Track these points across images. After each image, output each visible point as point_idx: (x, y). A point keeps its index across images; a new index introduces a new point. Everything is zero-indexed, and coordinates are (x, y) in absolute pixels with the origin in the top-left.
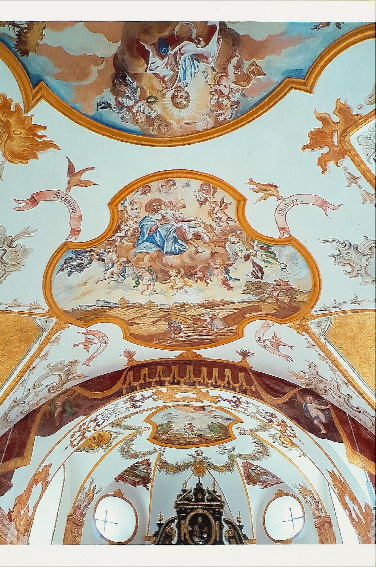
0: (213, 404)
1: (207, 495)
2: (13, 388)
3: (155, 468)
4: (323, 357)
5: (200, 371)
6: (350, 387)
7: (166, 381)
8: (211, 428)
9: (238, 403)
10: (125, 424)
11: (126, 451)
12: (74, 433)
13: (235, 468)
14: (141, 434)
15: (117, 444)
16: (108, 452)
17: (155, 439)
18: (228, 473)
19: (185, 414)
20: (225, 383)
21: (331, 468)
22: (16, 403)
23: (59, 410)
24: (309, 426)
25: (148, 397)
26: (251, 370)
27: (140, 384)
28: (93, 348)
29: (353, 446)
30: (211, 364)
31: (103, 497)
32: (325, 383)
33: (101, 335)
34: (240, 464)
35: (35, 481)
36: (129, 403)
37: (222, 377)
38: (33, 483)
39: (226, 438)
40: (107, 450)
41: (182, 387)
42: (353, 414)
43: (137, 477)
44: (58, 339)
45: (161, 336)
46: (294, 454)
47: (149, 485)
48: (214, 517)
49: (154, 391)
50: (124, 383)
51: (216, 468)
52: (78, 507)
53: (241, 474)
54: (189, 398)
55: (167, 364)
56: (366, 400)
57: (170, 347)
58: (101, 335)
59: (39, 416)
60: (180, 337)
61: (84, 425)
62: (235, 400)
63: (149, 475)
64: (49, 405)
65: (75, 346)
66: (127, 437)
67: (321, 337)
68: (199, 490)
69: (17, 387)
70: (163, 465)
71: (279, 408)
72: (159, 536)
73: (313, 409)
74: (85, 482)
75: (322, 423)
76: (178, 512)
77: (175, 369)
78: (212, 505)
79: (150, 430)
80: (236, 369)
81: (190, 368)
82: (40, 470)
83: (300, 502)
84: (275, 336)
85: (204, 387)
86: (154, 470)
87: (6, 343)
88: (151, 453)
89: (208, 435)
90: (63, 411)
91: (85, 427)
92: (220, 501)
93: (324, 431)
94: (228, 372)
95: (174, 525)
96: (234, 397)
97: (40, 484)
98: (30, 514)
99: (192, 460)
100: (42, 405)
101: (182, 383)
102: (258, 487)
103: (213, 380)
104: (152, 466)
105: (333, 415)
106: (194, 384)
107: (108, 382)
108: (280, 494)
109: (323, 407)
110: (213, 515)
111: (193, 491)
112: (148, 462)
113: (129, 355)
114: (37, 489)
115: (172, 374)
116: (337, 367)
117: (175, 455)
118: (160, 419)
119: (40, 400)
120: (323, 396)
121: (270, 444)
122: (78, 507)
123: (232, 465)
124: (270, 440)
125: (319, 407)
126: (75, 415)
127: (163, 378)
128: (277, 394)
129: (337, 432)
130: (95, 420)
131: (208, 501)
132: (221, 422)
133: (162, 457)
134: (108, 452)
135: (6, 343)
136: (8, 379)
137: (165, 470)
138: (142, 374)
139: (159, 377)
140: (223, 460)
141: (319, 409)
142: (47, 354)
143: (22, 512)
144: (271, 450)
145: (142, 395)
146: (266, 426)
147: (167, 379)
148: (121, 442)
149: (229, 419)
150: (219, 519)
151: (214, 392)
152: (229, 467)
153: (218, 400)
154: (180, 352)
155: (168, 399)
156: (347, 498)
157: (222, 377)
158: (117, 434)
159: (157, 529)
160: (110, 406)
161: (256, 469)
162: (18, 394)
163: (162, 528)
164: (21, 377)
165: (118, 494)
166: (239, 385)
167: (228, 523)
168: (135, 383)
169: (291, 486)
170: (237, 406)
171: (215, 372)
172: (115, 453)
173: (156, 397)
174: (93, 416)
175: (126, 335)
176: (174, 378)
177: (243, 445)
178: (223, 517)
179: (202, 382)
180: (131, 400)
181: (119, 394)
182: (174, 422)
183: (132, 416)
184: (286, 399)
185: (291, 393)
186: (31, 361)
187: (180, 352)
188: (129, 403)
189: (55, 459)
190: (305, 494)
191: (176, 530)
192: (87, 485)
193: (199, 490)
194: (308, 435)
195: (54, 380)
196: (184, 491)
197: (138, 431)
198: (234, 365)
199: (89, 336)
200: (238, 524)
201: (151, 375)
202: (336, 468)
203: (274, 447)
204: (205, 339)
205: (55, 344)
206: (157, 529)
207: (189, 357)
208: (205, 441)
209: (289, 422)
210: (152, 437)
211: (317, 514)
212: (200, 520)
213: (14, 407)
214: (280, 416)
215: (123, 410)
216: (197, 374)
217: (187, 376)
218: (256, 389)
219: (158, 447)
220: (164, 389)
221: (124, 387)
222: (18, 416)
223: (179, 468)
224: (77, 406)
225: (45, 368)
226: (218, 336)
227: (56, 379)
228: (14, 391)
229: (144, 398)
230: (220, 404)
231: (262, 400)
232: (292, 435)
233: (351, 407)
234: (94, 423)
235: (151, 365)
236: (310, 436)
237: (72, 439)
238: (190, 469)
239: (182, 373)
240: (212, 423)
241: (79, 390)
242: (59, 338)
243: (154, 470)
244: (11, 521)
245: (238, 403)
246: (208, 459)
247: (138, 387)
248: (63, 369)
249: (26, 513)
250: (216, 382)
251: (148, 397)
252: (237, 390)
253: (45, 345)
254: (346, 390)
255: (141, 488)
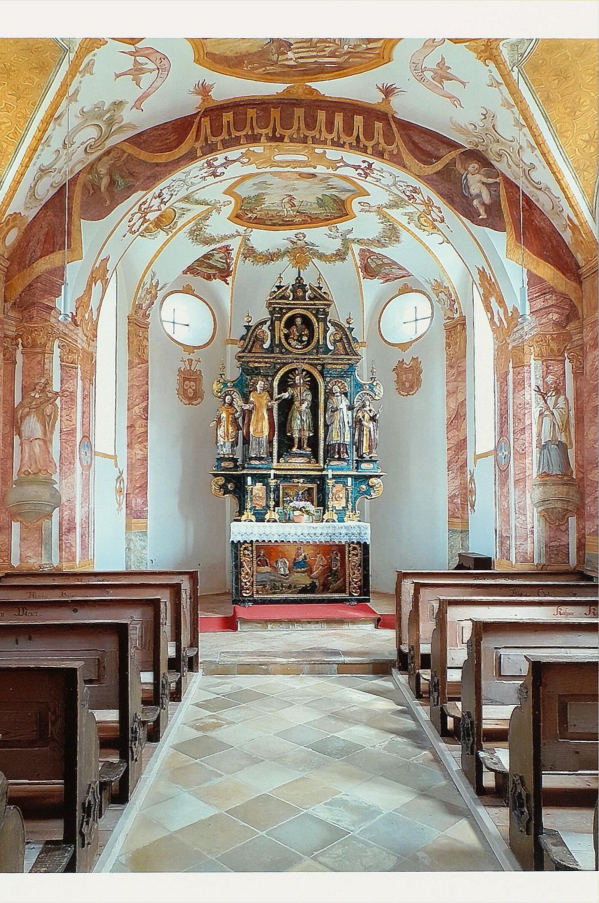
0: (331, 171)
1: (309, 292)
2: (35, 150)
3: (238, 258)
4: (508, 103)
5: (314, 119)
6: (538, 152)
7: (261, 135)
8: (321, 203)
9: (368, 171)
10: (196, 197)
11: (197, 235)
12: (133, 215)
13: (349, 257)
14: (219, 211)
15: (184, 226)
16: (172, 237)
17: (237, 217)
18: (338, 263)
19: (284, 183)
20: (352, 140)
21: (482, 263)
22: (44, 171)
23: (105, 182)
24: (464, 205)
25: (235, 161)
26: (393, 117)
27: (221, 141)
28: (147, 79)
29: (518, 239)
30: (334, 106)
31: (172, 293)
32: (503, 143)
33: (159, 56)
34: (357, 252)
35: (93, 280)
36: (206, 170)
37: (349, 128)
38: (91, 281)
39: (341, 217)
40: (171, 234)
41: (286, 145)
42: (530, 192)
43: (212, 267)
44: (91, 64)
45: (256, 58)
46: (433, 240)
47: (229, 279)
48: (316, 317)
49: (244, 151)
50: (197, 138)
51: (322, 257)
52: (140, 307)
53: (356, 264)
54: (295, 161)
55: (263, 105)
56: (554, 173)
57: (269, 77)
58: (159, 56)
59: (78, 189)
60: (287, 59)
61: (144, 203)
62: (363, 165)
63: (229, 267)
64: (88, 173)
65: (118, 76)
66: (199, 215)
67: (515, 69)
68: (299, 285)
69: (40, 147)
70: (249, 253)
71: (428, 180)
72: (247, 340)
73: (475, 182)
74: (143, 276)
75: (484, 204)
76: (271, 313)
77: (275, 113)
78: (315, 304)
79: (232, 206)
80: (374, 115)
81: (299, 112)
82: (97, 265)
83: (430, 300)
84: (442, 64)
85: (321, 146)
86: (237, 260)
87: (8, 71)
88: (233, 236)
89: (316, 211)
90: (112, 183)
91: (146, 206)
92: (327, 300)
93: (484, 216)
94: (358, 120)
95: (265, 328)
96: (364, 162)
97: (99, 282)
98: (95, 318)
99: (290, 245)
100: (78, 174)
101: (286, 140)
102: (377, 283)
103: (334, 135)
104: (234, 254)
105: (503, 192)
106: (304, 140)
107: (173, 137)
108: (405, 290)
109: (491, 181)
110: (316, 315)
111: (291, 287)
112: (227, 250)
113: (204, 90)
114: (97, 288)
115: (271, 125)
116: (526, 119)
117: (265, 240)
118: (246, 190)
119: (75, 165)
120: (493, 162)
121: (402, 226)
122: (140, 307)
123: (346, 253)
124: (404, 220)
125: (484, 180)
126: (130, 190)
127: (257, 131)
128: (427, 158)
129: (501, 217)
130: (159, 196)
131: (311, 299)
132: (336, 194)
133: (248, 242)
134: (172, 237)
135: (8, 71)
136: (25, 136)
137: (251, 259)
138: (224, 122)
139: (252, 128)
140: (336, 245)
141: (483, 183)
142: (77, 91)
143: (87, 316)
144: (404, 235)
145: (226, 158)
146: (402, 201)
147: (264, 131)
148: (189, 222)
149: (349, 191)
150: (324, 320)
151: (333, 154)
152: (340, 256)
153: (338, 165)
154: (285, 86)
155: (263, 162)
156: (493, 300)
157: (349, 128)
158: (184, 211)
159: (244, 332)
160: (178, 175)
161: (378, 258)
162: (45, 157)
163: (251, 331)
164: (45, 131)
165: (188, 290)
166: (372, 143)
167: (335, 324)
168: (214, 139)
169: (421, 280)
170: (367, 175)
171: (339, 119)
172: (182, 238)
173: (246, 160)
174: (156, 190)
175: (199, 55)
176: (274, 131)
177: (364, 225)
178: (328, 318)
179: (317, 137)
180: (210, 165)
181: (191, 157)
182: (267, 194)
183: (208, 185)
184: (439, 166)
185: (450, 156)
186: (55, 105)
187: (285, 86)
188: (206, 170)
189: (112, 251)
190: (440, 291)
191: (269, 333)
192: (147, 279)
193: (299, 285)
194: (459, 217)
195: (91, 133)
196: (279, 287)
197: (214, 207)
198: (369, 108)
199: (141, 60)
200: (347, 326)
201: (239, 124)
202: (489, 265)
203: (408, 231)
204: (327, 63)
205: (87, 75)
206: (244, 332)
207: (299, 92)
208: (312, 221)
209: (437, 201)
210: (235, 214)
211: (449, 314)
212: (299, 321)
213: (41, 177)
214: (427, 192)
215: (198, 180)
216: (311, 124)
217: (295, 127)
218: (399, 150)
219: (241, 229)
220: (258, 149)
221: (198, 145)
222: (48, 191)
223: (271, 257)
224: (132, 174)
225: (77, 117)
226: (349, 58)
227: (93, 133)
228: (37, 153)
229: (228, 162)
230: (342, 171)
231: (404, 167)
232: (439, 219)
233: (530, 180)
234: (158, 200)
235: (238, 106)
236: (463, 222)
237: (131, 223)
238: (286, 259)
239: (287, 123)
240: (323, 195)
241: (131, 150)
242: (93, 64)
243: (237, 260)
244: (77, 326)
245: (368, 171)
246: (313, 245)
247: (219, 146)
248: (104, 116)
249: (91, 317)
250: (339, 138)
251: (235, 161)
252: (370, 150)
253: (73, 77)
254: (530, 157)
255: (217, 283)
